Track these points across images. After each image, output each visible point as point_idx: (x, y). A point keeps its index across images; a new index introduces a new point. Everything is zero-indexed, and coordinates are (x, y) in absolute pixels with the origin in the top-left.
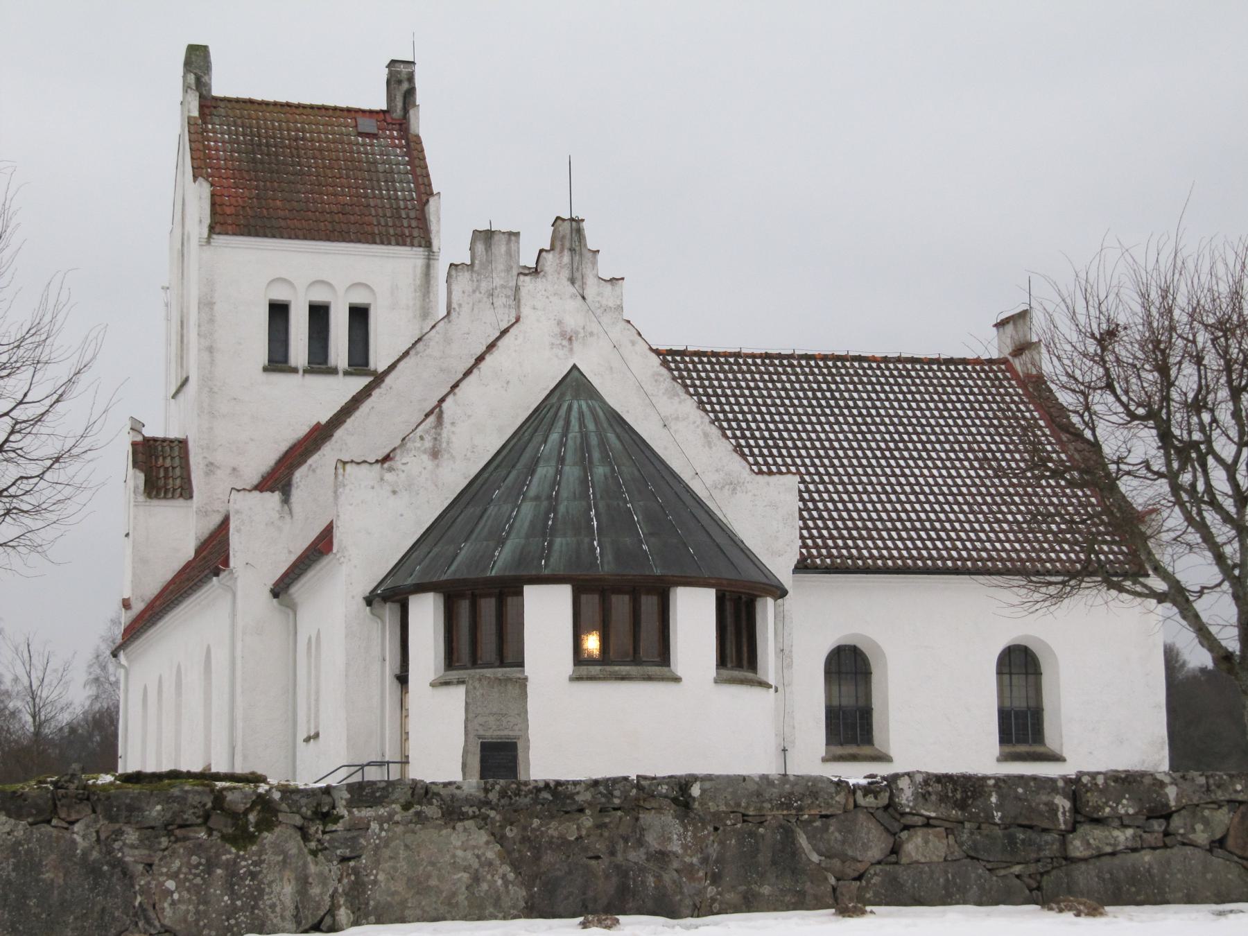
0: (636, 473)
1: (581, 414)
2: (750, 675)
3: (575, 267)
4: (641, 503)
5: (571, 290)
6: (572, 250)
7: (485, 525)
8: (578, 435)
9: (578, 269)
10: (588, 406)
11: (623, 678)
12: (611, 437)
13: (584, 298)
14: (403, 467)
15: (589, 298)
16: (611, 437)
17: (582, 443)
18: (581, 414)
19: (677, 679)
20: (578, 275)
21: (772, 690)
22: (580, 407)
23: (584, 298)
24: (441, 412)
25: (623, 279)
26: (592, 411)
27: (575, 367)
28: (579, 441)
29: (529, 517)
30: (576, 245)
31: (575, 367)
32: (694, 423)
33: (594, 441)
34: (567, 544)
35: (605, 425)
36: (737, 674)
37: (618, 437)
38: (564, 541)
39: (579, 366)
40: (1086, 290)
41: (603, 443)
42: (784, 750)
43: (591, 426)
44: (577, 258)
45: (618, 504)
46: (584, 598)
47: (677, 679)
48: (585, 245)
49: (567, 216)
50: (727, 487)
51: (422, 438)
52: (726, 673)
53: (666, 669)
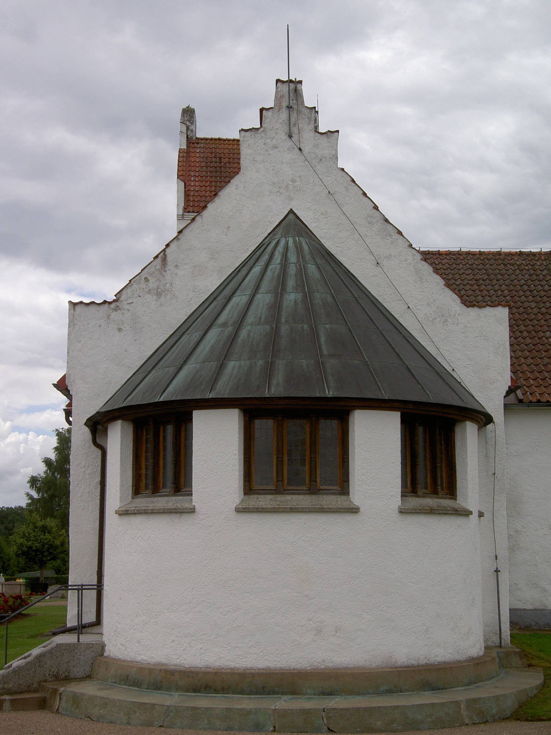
0: (329, 299)
1: (286, 248)
2: (447, 503)
3: (292, 122)
4: (327, 326)
5: (290, 143)
6: (289, 107)
7: (171, 356)
8: (278, 267)
9: (295, 125)
10: (295, 241)
11: (293, 510)
12: (312, 269)
13: (300, 149)
14: (127, 307)
15: (306, 150)
16: (312, 269)
17: (279, 275)
18: (286, 248)
19: (355, 510)
20: (295, 130)
21: (474, 517)
22: (287, 242)
23: (300, 149)
24: (165, 255)
25: (338, 131)
26: (299, 249)
27: (291, 211)
28: (277, 271)
29: (212, 342)
30: (293, 103)
31: (291, 211)
32: (406, 260)
33: (292, 270)
34: (240, 367)
35: (308, 257)
36: (430, 502)
37: (319, 268)
38: (237, 364)
39: (296, 211)
40: (517, 647)
41: (302, 272)
42: (497, 571)
43: (293, 258)
44: (294, 115)
45: (302, 328)
46: (258, 423)
47: (355, 510)
48: (303, 102)
49: (285, 79)
50: (438, 320)
51: (146, 280)
52: (414, 502)
53: (344, 498)
